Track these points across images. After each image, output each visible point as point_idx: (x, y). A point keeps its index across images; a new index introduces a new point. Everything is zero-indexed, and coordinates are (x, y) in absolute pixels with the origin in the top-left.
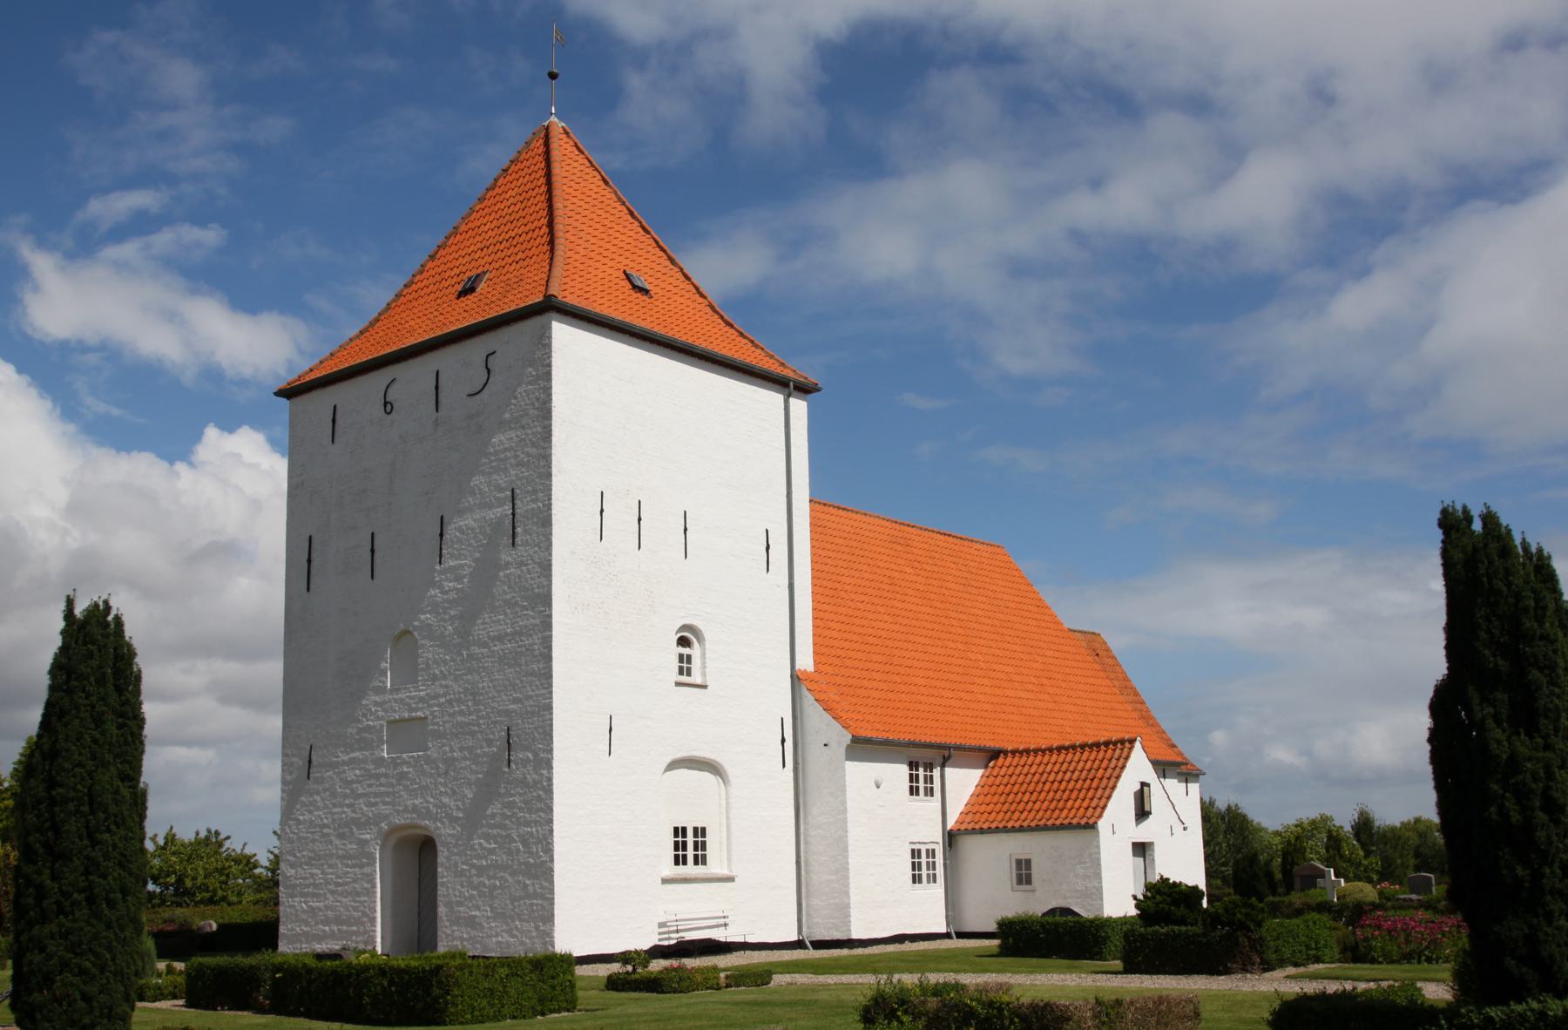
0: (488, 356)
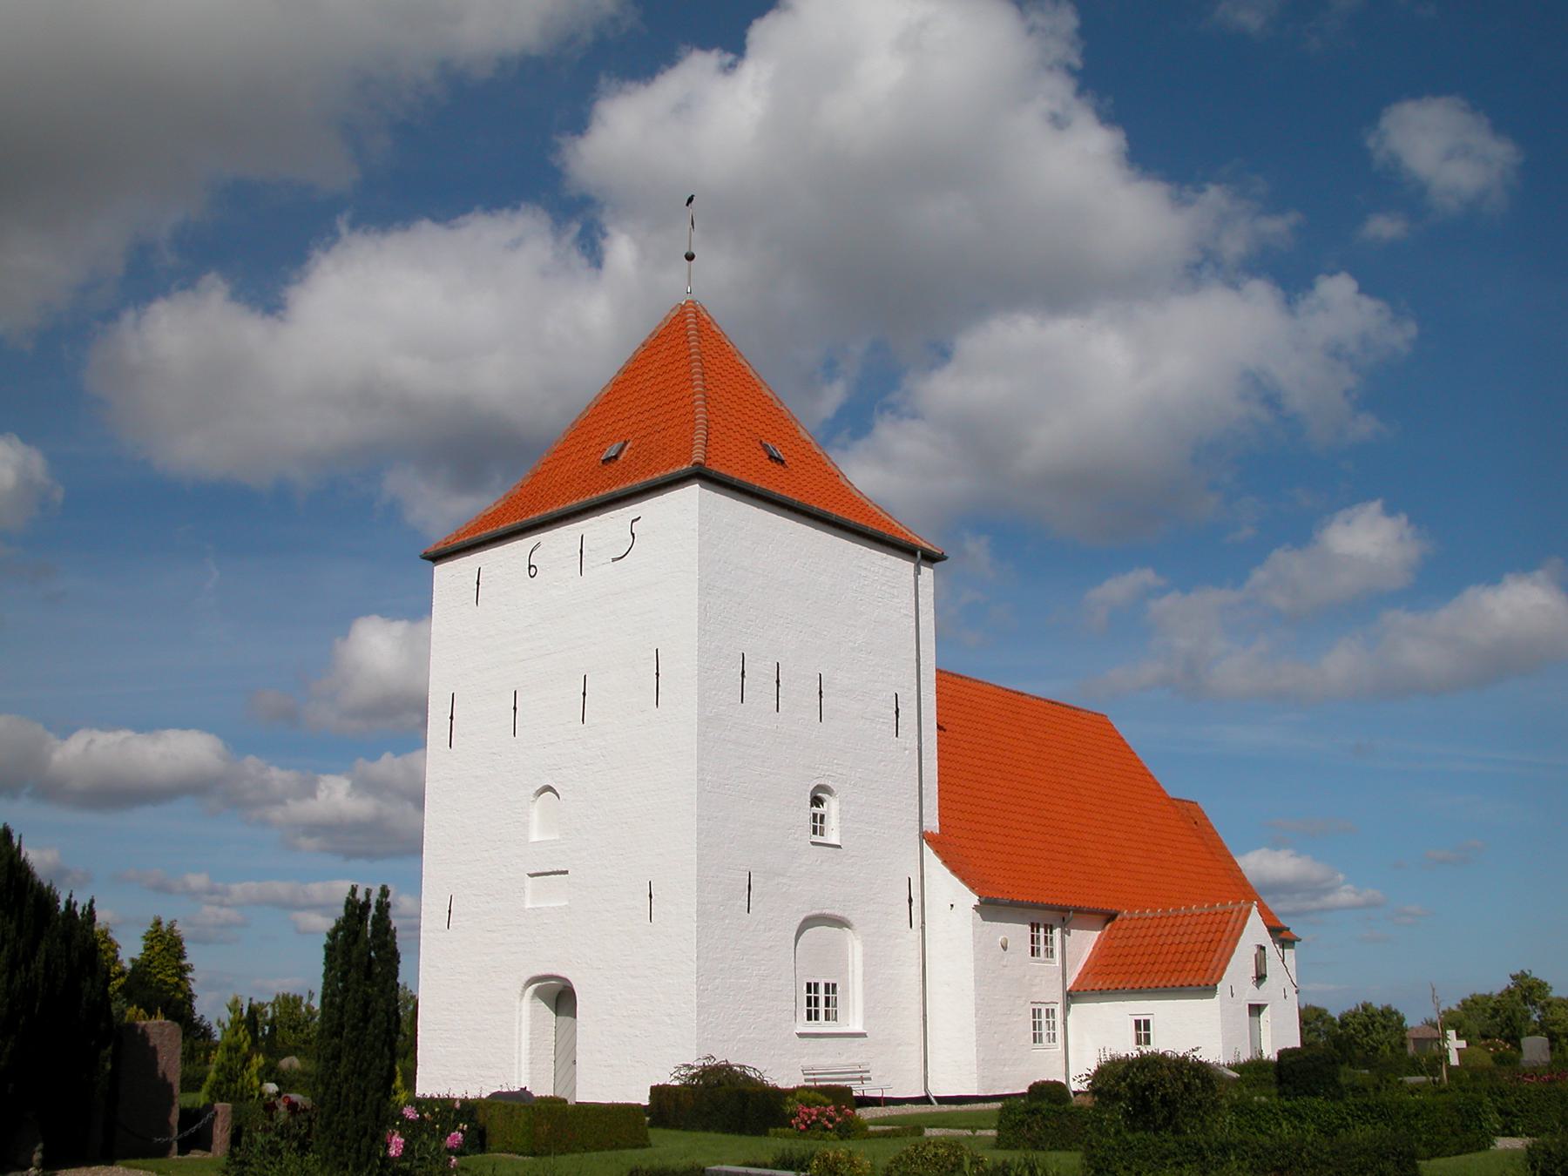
0: (633, 521)
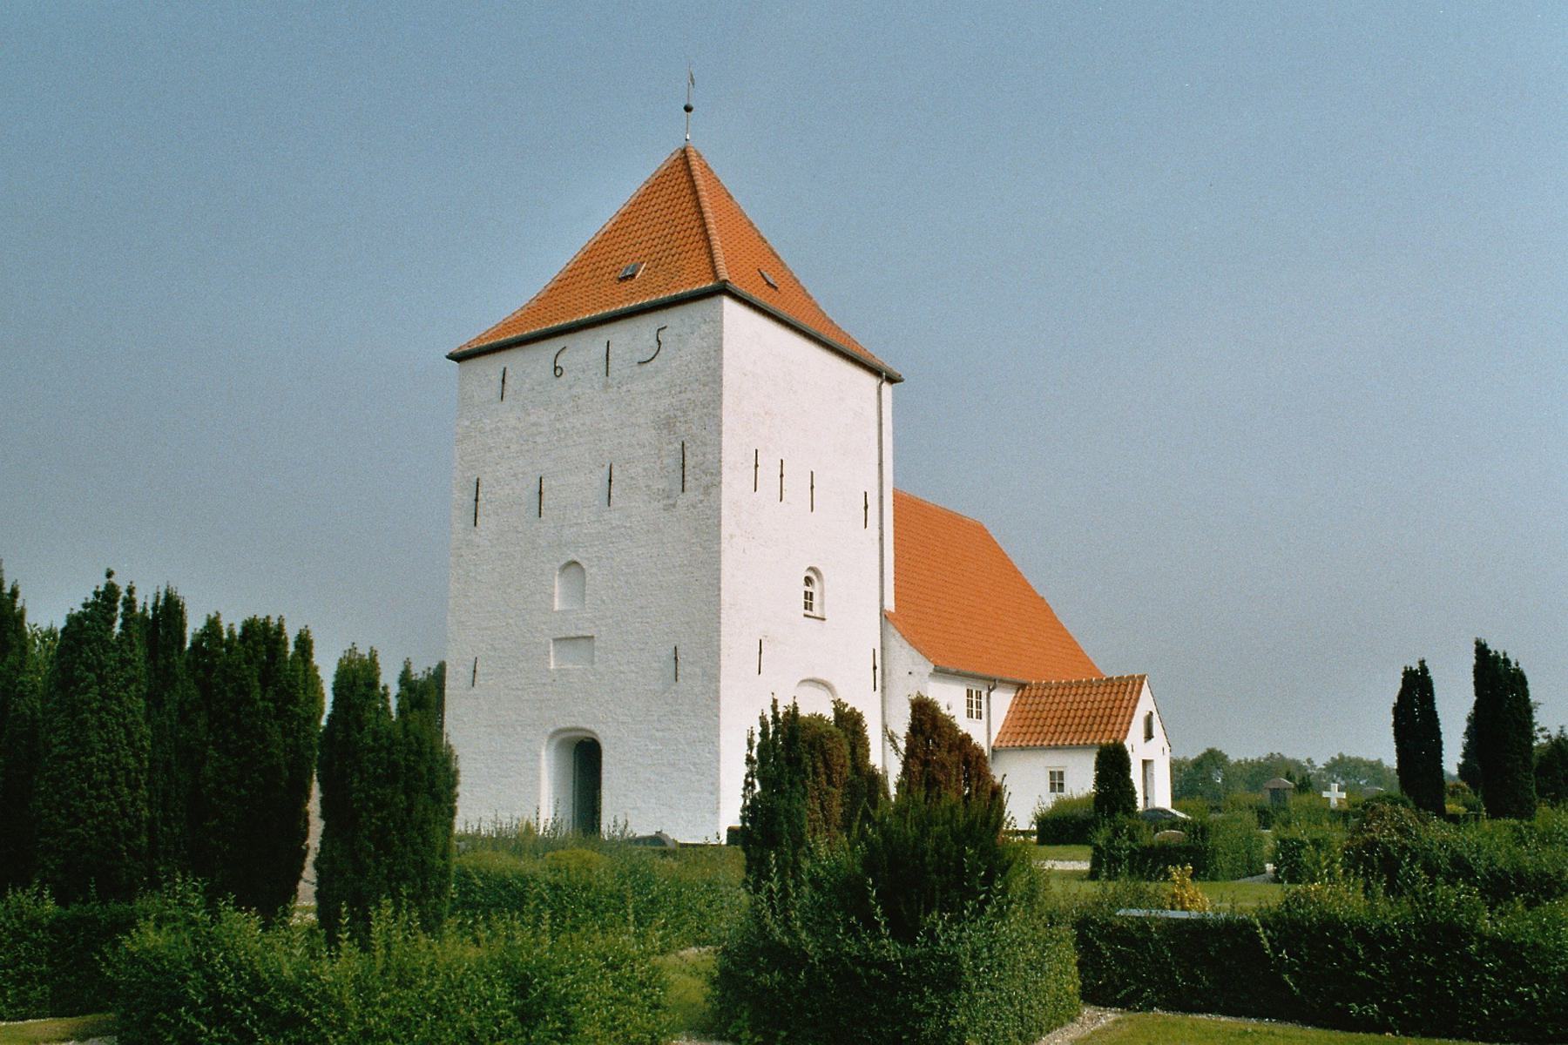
0: (659, 330)
